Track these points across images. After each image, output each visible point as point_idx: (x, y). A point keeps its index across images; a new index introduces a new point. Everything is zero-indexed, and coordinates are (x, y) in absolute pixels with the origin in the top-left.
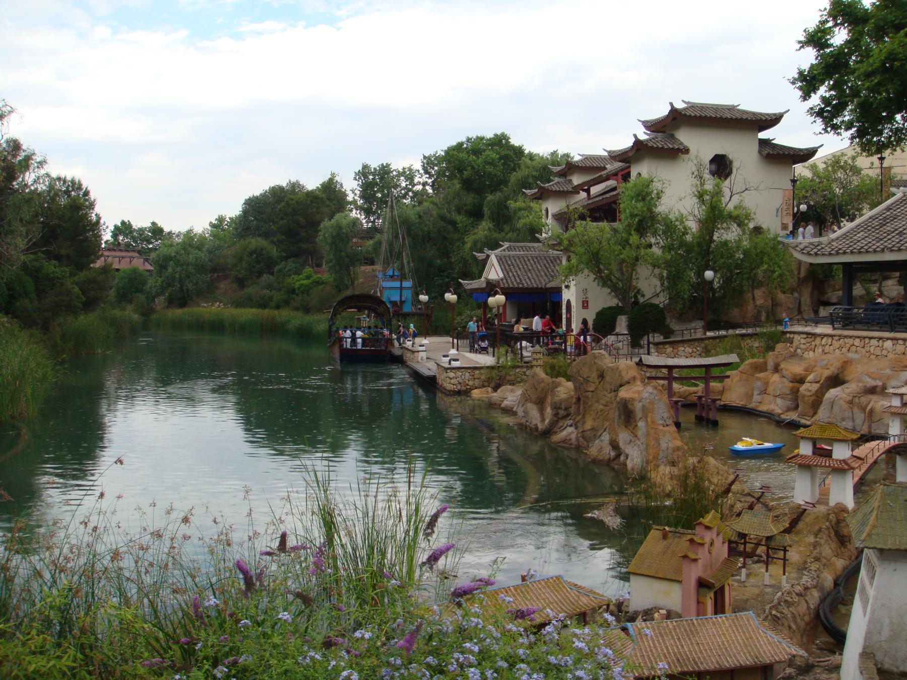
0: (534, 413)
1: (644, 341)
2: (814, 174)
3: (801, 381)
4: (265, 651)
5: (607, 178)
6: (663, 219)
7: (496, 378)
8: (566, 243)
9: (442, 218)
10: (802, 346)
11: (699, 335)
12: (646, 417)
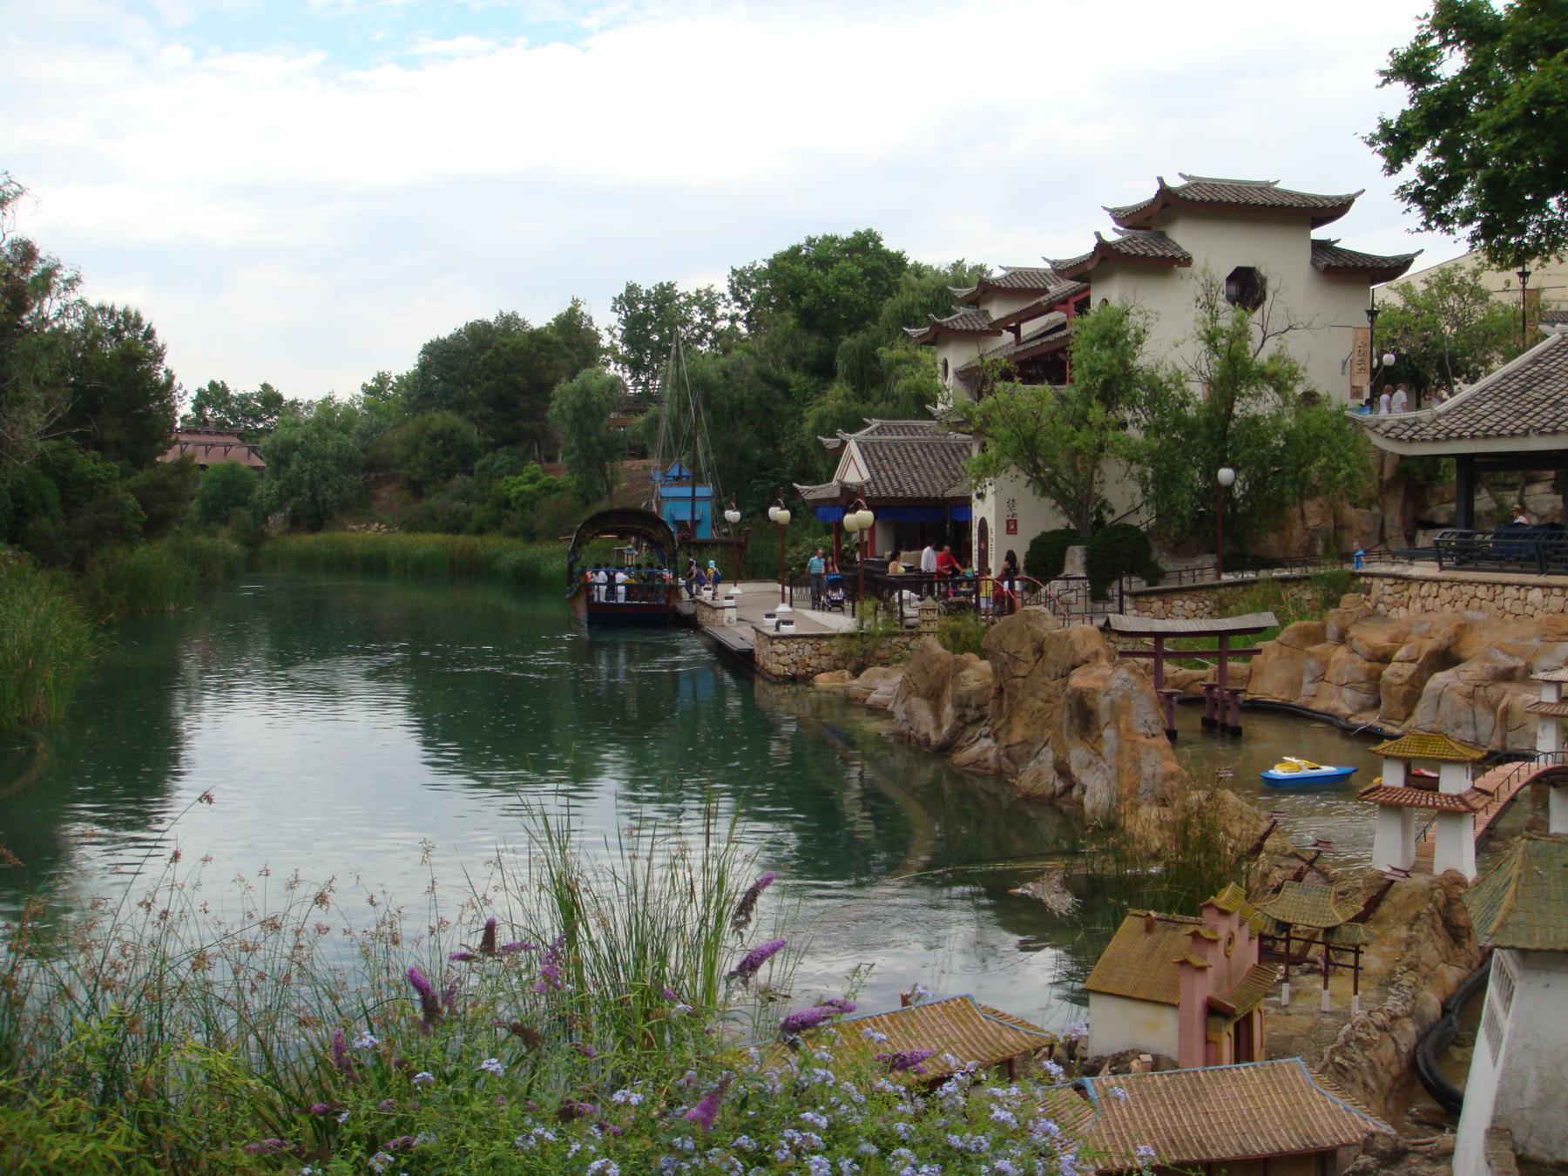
0: (923, 714)
1: (1113, 591)
2: (1407, 301)
3: (1385, 659)
4: (458, 1125)
5: (1050, 309)
6: (1147, 378)
7: (858, 654)
8: (978, 419)
9: (764, 377)
10: (1387, 599)
11: (1208, 579)
12: (1117, 721)
